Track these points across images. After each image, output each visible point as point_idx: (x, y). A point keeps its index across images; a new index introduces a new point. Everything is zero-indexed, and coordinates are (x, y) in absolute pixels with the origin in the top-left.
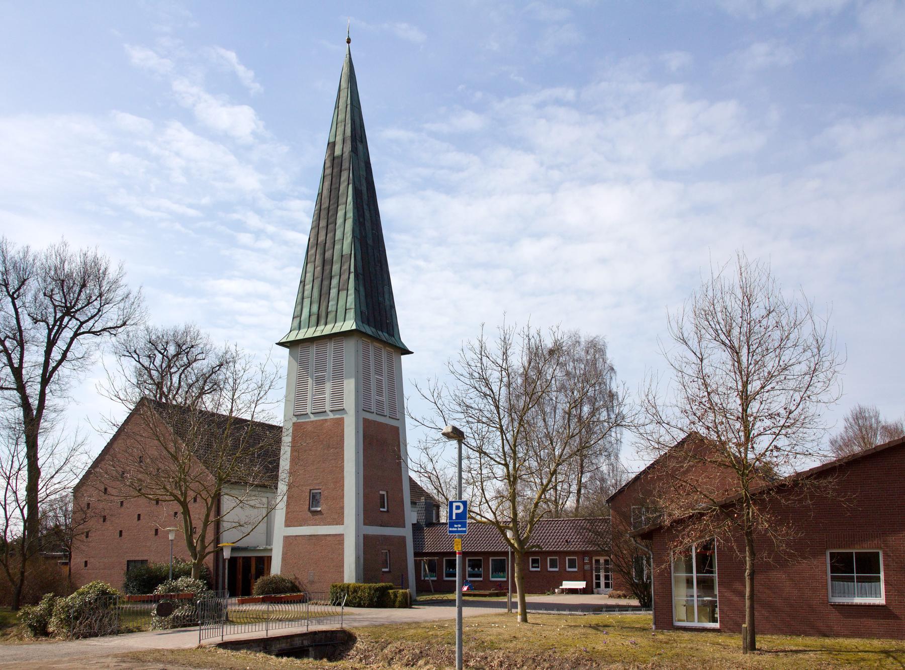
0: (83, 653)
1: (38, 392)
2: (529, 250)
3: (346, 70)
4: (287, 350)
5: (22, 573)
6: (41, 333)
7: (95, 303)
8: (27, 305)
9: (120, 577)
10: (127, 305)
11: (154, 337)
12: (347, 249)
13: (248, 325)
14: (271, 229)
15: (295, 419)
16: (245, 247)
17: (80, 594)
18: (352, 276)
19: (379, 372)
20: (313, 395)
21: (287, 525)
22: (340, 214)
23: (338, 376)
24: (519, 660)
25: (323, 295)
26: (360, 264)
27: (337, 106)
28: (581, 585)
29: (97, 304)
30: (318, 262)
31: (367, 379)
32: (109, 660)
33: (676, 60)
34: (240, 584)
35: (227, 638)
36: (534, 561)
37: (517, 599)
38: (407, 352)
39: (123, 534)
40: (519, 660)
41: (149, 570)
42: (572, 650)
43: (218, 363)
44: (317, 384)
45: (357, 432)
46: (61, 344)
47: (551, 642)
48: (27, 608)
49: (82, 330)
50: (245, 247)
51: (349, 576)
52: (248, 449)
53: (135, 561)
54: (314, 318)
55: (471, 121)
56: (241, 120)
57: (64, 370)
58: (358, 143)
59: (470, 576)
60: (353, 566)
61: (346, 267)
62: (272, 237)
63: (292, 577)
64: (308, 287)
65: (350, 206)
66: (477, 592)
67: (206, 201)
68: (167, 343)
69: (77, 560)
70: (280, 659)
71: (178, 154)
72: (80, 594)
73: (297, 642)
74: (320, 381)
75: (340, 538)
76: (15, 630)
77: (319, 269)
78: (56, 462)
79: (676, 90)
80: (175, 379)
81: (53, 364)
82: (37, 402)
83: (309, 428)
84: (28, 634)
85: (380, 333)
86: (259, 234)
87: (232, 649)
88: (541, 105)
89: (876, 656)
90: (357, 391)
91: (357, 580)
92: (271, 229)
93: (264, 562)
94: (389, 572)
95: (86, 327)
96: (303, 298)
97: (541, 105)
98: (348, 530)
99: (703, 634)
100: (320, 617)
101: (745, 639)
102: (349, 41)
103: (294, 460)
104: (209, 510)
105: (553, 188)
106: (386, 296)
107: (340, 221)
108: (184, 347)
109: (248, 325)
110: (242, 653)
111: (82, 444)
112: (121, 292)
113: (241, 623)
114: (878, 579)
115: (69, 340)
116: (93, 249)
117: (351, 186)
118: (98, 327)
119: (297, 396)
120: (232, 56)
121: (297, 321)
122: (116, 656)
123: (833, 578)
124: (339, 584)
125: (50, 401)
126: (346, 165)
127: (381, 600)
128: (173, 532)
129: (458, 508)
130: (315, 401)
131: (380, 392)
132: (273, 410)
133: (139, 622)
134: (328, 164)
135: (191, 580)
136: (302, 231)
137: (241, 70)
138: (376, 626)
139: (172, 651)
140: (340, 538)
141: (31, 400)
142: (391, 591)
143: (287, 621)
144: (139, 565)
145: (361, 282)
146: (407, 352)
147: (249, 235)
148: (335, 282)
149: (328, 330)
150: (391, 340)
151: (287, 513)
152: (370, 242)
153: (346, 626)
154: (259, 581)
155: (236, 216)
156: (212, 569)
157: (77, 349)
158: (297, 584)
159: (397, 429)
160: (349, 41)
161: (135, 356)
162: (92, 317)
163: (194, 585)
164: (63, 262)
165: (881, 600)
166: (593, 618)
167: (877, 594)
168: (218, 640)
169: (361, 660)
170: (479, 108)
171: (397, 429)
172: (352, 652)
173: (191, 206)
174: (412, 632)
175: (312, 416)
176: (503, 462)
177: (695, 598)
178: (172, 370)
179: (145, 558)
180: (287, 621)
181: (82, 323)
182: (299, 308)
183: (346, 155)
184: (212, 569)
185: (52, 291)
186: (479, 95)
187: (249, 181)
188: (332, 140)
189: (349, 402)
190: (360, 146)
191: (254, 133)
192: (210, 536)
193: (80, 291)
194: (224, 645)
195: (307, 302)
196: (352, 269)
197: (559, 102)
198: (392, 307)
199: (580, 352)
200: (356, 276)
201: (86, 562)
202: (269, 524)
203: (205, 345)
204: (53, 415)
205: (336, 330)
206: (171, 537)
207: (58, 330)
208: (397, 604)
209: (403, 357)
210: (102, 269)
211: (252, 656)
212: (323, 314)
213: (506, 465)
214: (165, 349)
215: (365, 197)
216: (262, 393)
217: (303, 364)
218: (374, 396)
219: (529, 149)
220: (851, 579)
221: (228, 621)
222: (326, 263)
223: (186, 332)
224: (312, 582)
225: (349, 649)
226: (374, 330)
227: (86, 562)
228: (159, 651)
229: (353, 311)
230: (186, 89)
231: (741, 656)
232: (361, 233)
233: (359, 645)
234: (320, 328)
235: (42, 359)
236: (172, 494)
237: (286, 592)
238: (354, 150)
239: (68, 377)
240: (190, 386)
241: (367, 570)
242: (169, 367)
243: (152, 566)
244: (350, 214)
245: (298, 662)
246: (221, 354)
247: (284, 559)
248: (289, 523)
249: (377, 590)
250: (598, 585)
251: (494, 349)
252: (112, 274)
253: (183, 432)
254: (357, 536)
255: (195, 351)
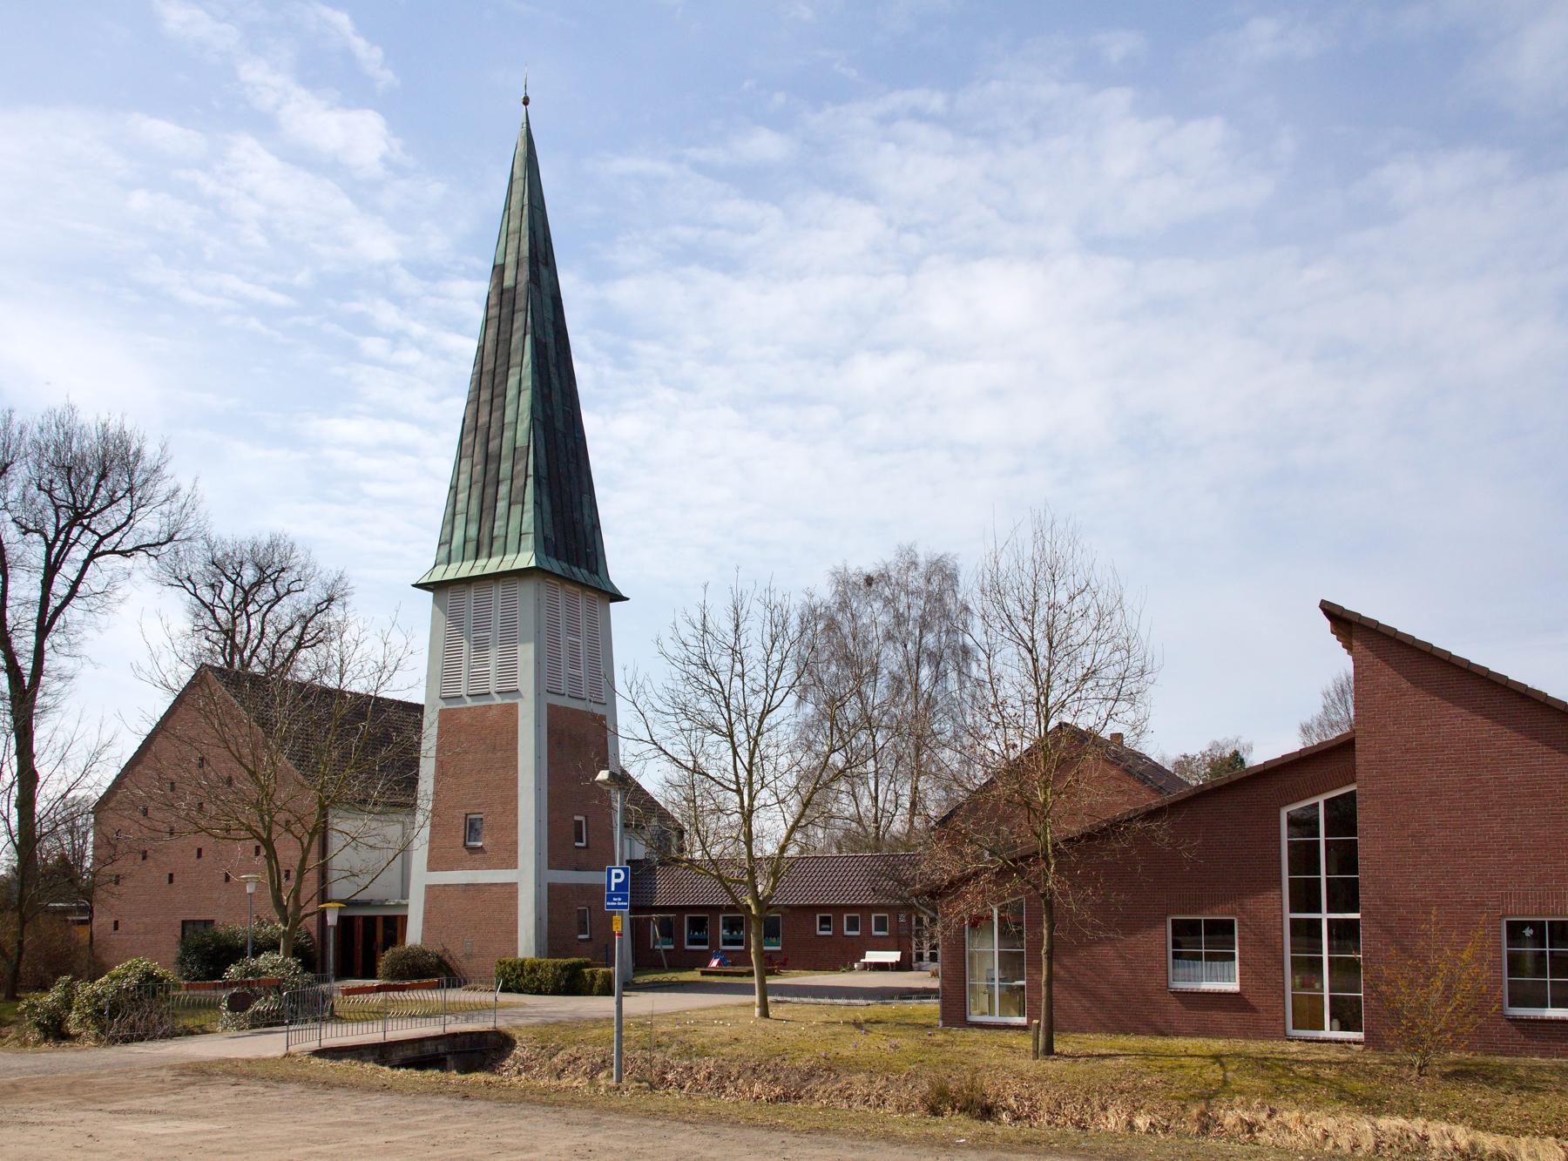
0: (126, 1064)
1: (32, 647)
2: (869, 373)
3: (522, 149)
4: (431, 594)
5: (20, 943)
6: (35, 552)
7: (122, 501)
8: (11, 506)
9: (171, 947)
10: (175, 506)
11: (219, 554)
12: (522, 440)
13: (372, 551)
14: (418, 329)
15: (442, 705)
16: (374, 362)
17: (114, 978)
18: (530, 481)
19: (575, 632)
20: (470, 667)
21: (431, 868)
22: (513, 381)
23: (509, 638)
24: (734, 1072)
25: (486, 510)
26: (543, 462)
27: (507, 207)
28: (893, 957)
29: (125, 505)
30: (479, 457)
31: (554, 643)
32: (163, 1072)
33: (1119, 45)
34: (359, 960)
35: (327, 1043)
36: (825, 921)
37: (755, 980)
38: (619, 598)
39: (175, 878)
40: (734, 1072)
41: (216, 938)
42: (807, 1056)
43: (325, 596)
44: (477, 649)
45: (538, 726)
46: (68, 571)
47: (782, 1046)
48: (33, 997)
49: (102, 548)
50: (374, 362)
51: (526, 946)
52: (370, 742)
53: (194, 922)
54: (471, 547)
55: (766, 145)
56: (361, 136)
57: (73, 612)
58: (542, 268)
59: (725, 943)
60: (532, 932)
61: (520, 467)
62: (420, 345)
63: (438, 949)
64: (463, 496)
65: (527, 370)
66: (730, 969)
67: (302, 278)
68: (241, 564)
69: (102, 920)
70: (395, 1071)
71: (251, 194)
72: (114, 978)
73: (430, 1048)
74: (481, 646)
75: (511, 889)
76: (13, 1032)
77: (479, 468)
78: (69, 773)
79: (1119, 98)
80: (255, 622)
81: (55, 603)
82: (30, 665)
83: (465, 719)
84: (34, 1035)
85: (575, 569)
86: (396, 338)
87: (332, 1058)
88: (886, 120)
89: (1201, 1062)
90: (538, 663)
91: (539, 953)
92: (418, 329)
93: (395, 926)
94: (590, 940)
95: (107, 545)
96: (454, 515)
97: (886, 120)
98: (525, 876)
99: (1002, 1033)
100: (470, 1011)
101: (1036, 1039)
102: (526, 102)
103: (441, 768)
104: (306, 852)
105: (911, 266)
106: (586, 511)
107: (511, 393)
108: (269, 572)
109: (372, 551)
110: (344, 1063)
111: (109, 744)
112: (163, 489)
113: (352, 1021)
114: (1231, 957)
115: (80, 565)
116: (118, 416)
117: (528, 337)
118: (128, 545)
119: (445, 665)
120: (342, 19)
121: (445, 549)
122: (172, 1068)
123: (1176, 956)
124: (509, 959)
125: (51, 661)
126: (521, 302)
127: (572, 984)
128: (252, 882)
129: (618, 876)
130: (473, 677)
131: (575, 664)
132: (409, 683)
133: (204, 1018)
134: (493, 301)
135: (278, 958)
136: (470, 336)
137: (360, 45)
138: (547, 1025)
139: (249, 1061)
140: (511, 889)
141: (21, 662)
142: (586, 970)
143: (416, 1017)
144: (200, 928)
145: (545, 490)
146: (619, 598)
147: (379, 340)
148: (504, 489)
149: (492, 565)
150: (593, 581)
151: (431, 850)
152: (559, 425)
153: (502, 1024)
154: (387, 954)
155: (356, 307)
156: (315, 934)
157: (96, 577)
158: (446, 958)
159: (603, 717)
160: (526, 102)
161: (189, 585)
162: (119, 528)
163: (282, 965)
164: (68, 437)
165: (1233, 986)
166: (876, 1009)
167: (1230, 979)
168: (314, 1045)
169: (519, 1073)
170: (781, 123)
171: (603, 717)
172: (509, 1062)
173: (274, 287)
174: (596, 1032)
175: (468, 700)
176: (734, 787)
177: (996, 983)
178: (251, 609)
179: (209, 917)
180: (416, 1017)
181: (102, 538)
182: (448, 528)
183: (522, 287)
184: (315, 934)
185: (51, 481)
186: (780, 98)
187: (377, 244)
188: (499, 261)
189: (526, 680)
190: (544, 272)
191: (384, 160)
192: (311, 885)
193: (98, 486)
194: (322, 1053)
195: (460, 520)
196: (531, 471)
197: (918, 115)
198: (596, 526)
199: (916, 580)
200: (537, 483)
201: (116, 923)
202: (401, 864)
203: (304, 567)
204: (57, 685)
205: (505, 567)
206: (250, 889)
207: (62, 548)
208: (595, 989)
209: (612, 605)
210: (133, 449)
211: (358, 1067)
212: (486, 541)
213: (739, 792)
214: (238, 575)
215: (552, 353)
216: (384, 678)
217: (455, 618)
218: (565, 669)
219: (867, 196)
220: (1198, 957)
221: (334, 1018)
222: (490, 460)
223: (273, 546)
224: (469, 956)
225: (504, 1058)
226: (565, 565)
227: (116, 923)
228: (230, 1061)
229: (531, 537)
230: (263, 78)
231: (1028, 1065)
232: (544, 411)
233: (517, 1051)
234: (482, 562)
235: (37, 594)
236: (249, 828)
237: (434, 970)
238: (534, 278)
239: (80, 623)
240: (281, 635)
241: (554, 936)
242: (245, 602)
243: (222, 931)
244: (527, 383)
245: (418, 1074)
246: (329, 582)
247: (426, 920)
248: (433, 865)
249: (564, 968)
250: (920, 957)
251: (722, 623)
252: (151, 453)
253: (270, 719)
254: (538, 885)
255: (288, 577)
